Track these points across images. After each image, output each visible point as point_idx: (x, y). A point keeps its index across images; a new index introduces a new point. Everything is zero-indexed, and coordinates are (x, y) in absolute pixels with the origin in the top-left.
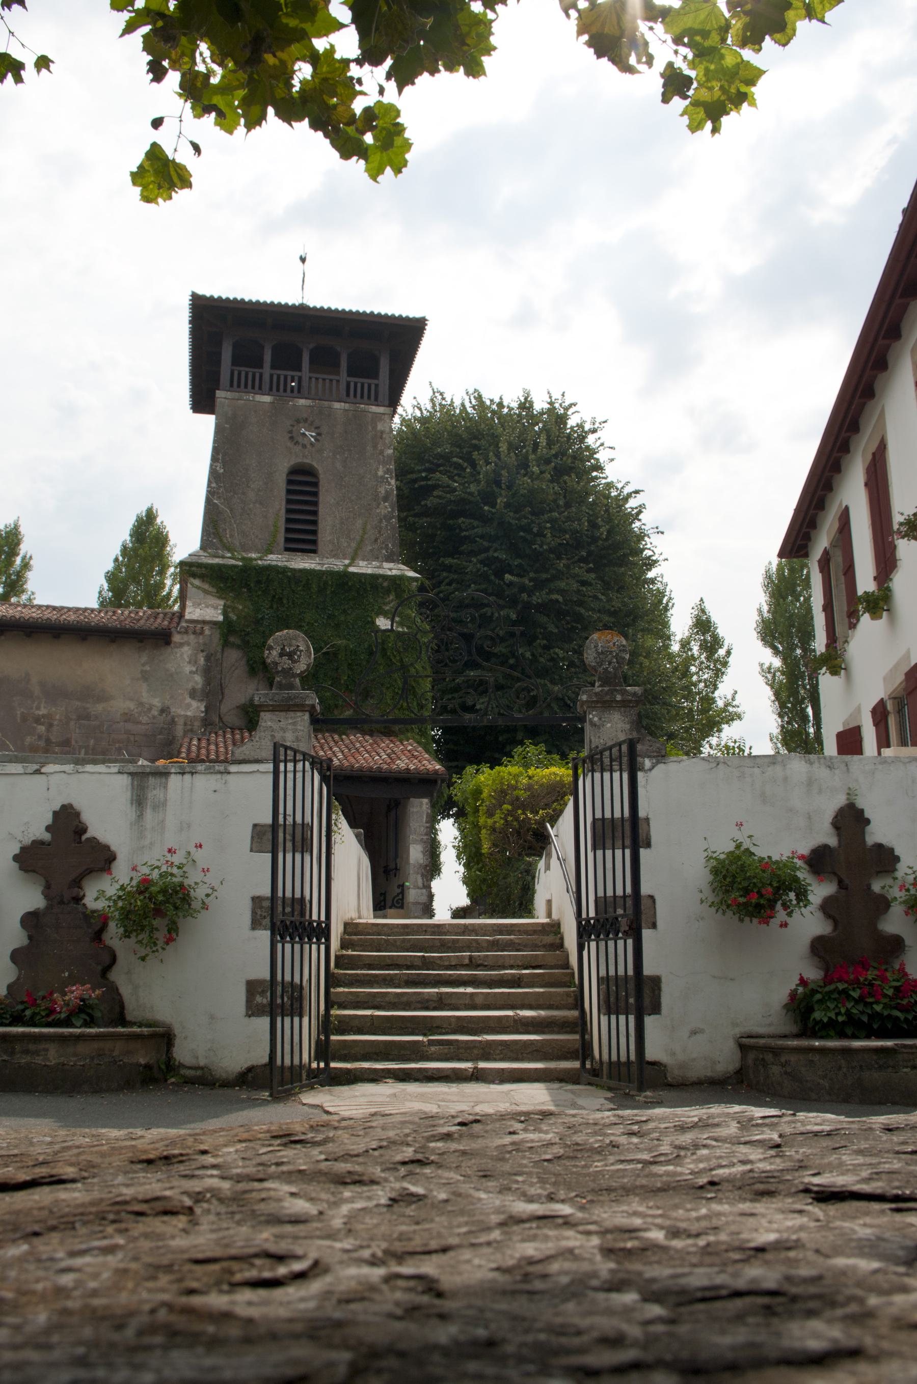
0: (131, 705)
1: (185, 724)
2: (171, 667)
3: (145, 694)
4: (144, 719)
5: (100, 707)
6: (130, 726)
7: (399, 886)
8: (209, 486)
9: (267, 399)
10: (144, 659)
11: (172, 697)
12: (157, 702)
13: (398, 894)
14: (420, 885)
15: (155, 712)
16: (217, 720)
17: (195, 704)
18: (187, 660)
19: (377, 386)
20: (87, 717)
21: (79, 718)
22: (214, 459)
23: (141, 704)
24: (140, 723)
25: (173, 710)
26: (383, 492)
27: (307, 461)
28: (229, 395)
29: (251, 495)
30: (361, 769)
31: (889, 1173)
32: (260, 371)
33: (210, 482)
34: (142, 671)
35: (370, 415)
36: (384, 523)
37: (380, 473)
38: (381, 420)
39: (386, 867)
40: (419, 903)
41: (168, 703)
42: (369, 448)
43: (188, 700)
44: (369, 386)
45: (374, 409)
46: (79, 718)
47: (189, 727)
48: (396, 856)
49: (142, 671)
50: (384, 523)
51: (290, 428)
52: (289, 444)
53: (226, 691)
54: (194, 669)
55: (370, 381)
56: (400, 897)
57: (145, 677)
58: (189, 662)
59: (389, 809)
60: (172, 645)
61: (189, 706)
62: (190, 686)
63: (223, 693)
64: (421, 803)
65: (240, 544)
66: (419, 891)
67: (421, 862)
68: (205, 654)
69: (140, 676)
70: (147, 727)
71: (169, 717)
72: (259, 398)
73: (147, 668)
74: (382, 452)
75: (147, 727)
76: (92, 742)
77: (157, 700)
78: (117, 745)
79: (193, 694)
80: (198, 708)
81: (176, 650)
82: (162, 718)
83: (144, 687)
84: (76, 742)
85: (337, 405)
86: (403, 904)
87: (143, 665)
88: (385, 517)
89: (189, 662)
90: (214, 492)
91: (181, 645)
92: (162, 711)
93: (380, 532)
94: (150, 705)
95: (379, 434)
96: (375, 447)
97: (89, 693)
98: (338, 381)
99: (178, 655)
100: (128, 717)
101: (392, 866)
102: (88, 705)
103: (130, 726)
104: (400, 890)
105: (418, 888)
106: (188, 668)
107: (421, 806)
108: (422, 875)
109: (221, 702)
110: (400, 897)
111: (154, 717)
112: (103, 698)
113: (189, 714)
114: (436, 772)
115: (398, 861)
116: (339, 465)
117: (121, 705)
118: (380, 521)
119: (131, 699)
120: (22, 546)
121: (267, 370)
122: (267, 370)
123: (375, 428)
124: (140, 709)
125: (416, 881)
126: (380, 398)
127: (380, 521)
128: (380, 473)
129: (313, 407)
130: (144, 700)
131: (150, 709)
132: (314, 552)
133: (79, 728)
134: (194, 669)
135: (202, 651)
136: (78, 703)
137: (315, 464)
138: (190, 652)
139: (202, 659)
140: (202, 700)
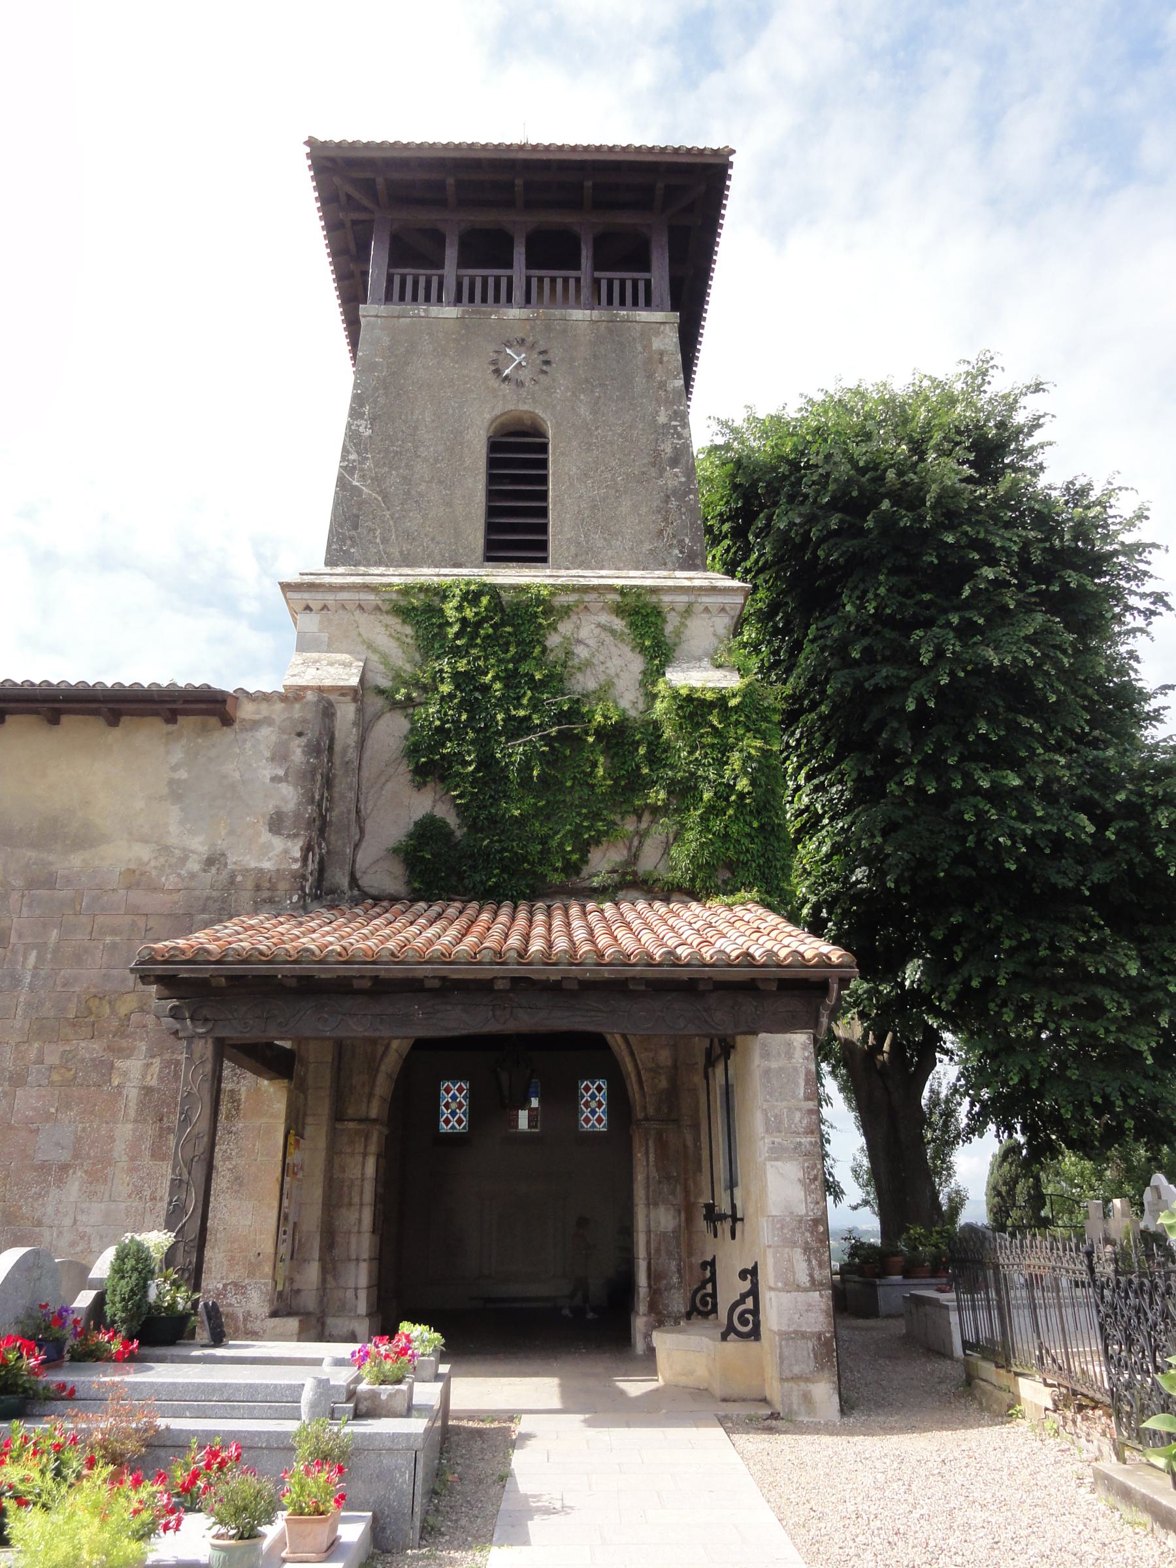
0: (144, 852)
1: (258, 888)
2: (232, 770)
3: (174, 829)
4: (170, 881)
5: (76, 861)
6: (138, 897)
7: (743, 1274)
8: (344, 458)
9: (450, 312)
10: (177, 755)
11: (231, 832)
12: (199, 845)
13: (744, 1297)
14: (804, 1280)
15: (194, 865)
16: (345, 882)
17: (278, 843)
18: (268, 754)
19: (648, 283)
20: (49, 882)
21: (32, 884)
22: (355, 413)
23: (166, 849)
24: (155, 888)
25: (232, 859)
26: (669, 450)
27: (526, 408)
28: (382, 309)
29: (421, 468)
30: (624, 960)
31: (358, 812)
32: (439, 272)
33: (345, 451)
34: (171, 782)
35: (638, 327)
36: (674, 503)
37: (662, 419)
38: (658, 333)
39: (710, 1208)
40: (803, 1335)
41: (221, 845)
42: (640, 380)
43: (266, 836)
44: (635, 283)
45: (643, 315)
46: (32, 884)
47: (266, 894)
48: (732, 1184)
49: (171, 782)
50: (674, 503)
51: (495, 356)
52: (494, 383)
53: (369, 825)
54: (281, 773)
55: (636, 275)
56: (749, 1303)
57: (176, 792)
58: (273, 759)
59: (710, 1062)
60: (236, 726)
61: (268, 847)
62: (270, 808)
63: (362, 832)
64: (789, 1044)
65: (401, 552)
66: (801, 1297)
67: (801, 1210)
68: (303, 741)
69: (166, 790)
70: (175, 897)
71: (224, 875)
72: (435, 311)
73: (183, 774)
74: (662, 385)
75: (175, 897)
76: (54, 934)
77: (201, 839)
78: (108, 939)
79: (276, 824)
80: (286, 851)
81: (245, 735)
82: (208, 877)
83: (173, 814)
84: (20, 936)
85: (578, 314)
86: (757, 1324)
87: (174, 769)
88: (675, 492)
89: (273, 759)
90: (354, 468)
91: (255, 725)
92: (210, 862)
93: (666, 519)
94: (184, 849)
95: (657, 357)
96: (650, 376)
97: (55, 832)
98: (578, 280)
99: (248, 745)
100: (135, 879)
101: (724, 1207)
102: (51, 858)
103: (138, 897)
104: (746, 1286)
105: (799, 1288)
106: (267, 771)
107: (789, 1056)
108: (807, 1249)
109: (357, 846)
110: (749, 1303)
111: (192, 876)
112: (85, 840)
113: (267, 865)
114: (824, 962)
115: (738, 1192)
116: (584, 411)
117: (120, 854)
118: (667, 499)
119: (144, 840)
120: (960, 1217)
121: (450, 270)
122: (450, 270)
123: (647, 346)
124: (162, 860)
125: (791, 1269)
126: (655, 299)
127: (667, 499)
128: (662, 419)
129: (534, 319)
130: (172, 841)
131: (184, 860)
132: (544, 560)
133: (30, 906)
134: (281, 773)
135: (300, 734)
136: (32, 854)
137: (539, 412)
138: (273, 738)
139: (299, 751)
140: (296, 836)
